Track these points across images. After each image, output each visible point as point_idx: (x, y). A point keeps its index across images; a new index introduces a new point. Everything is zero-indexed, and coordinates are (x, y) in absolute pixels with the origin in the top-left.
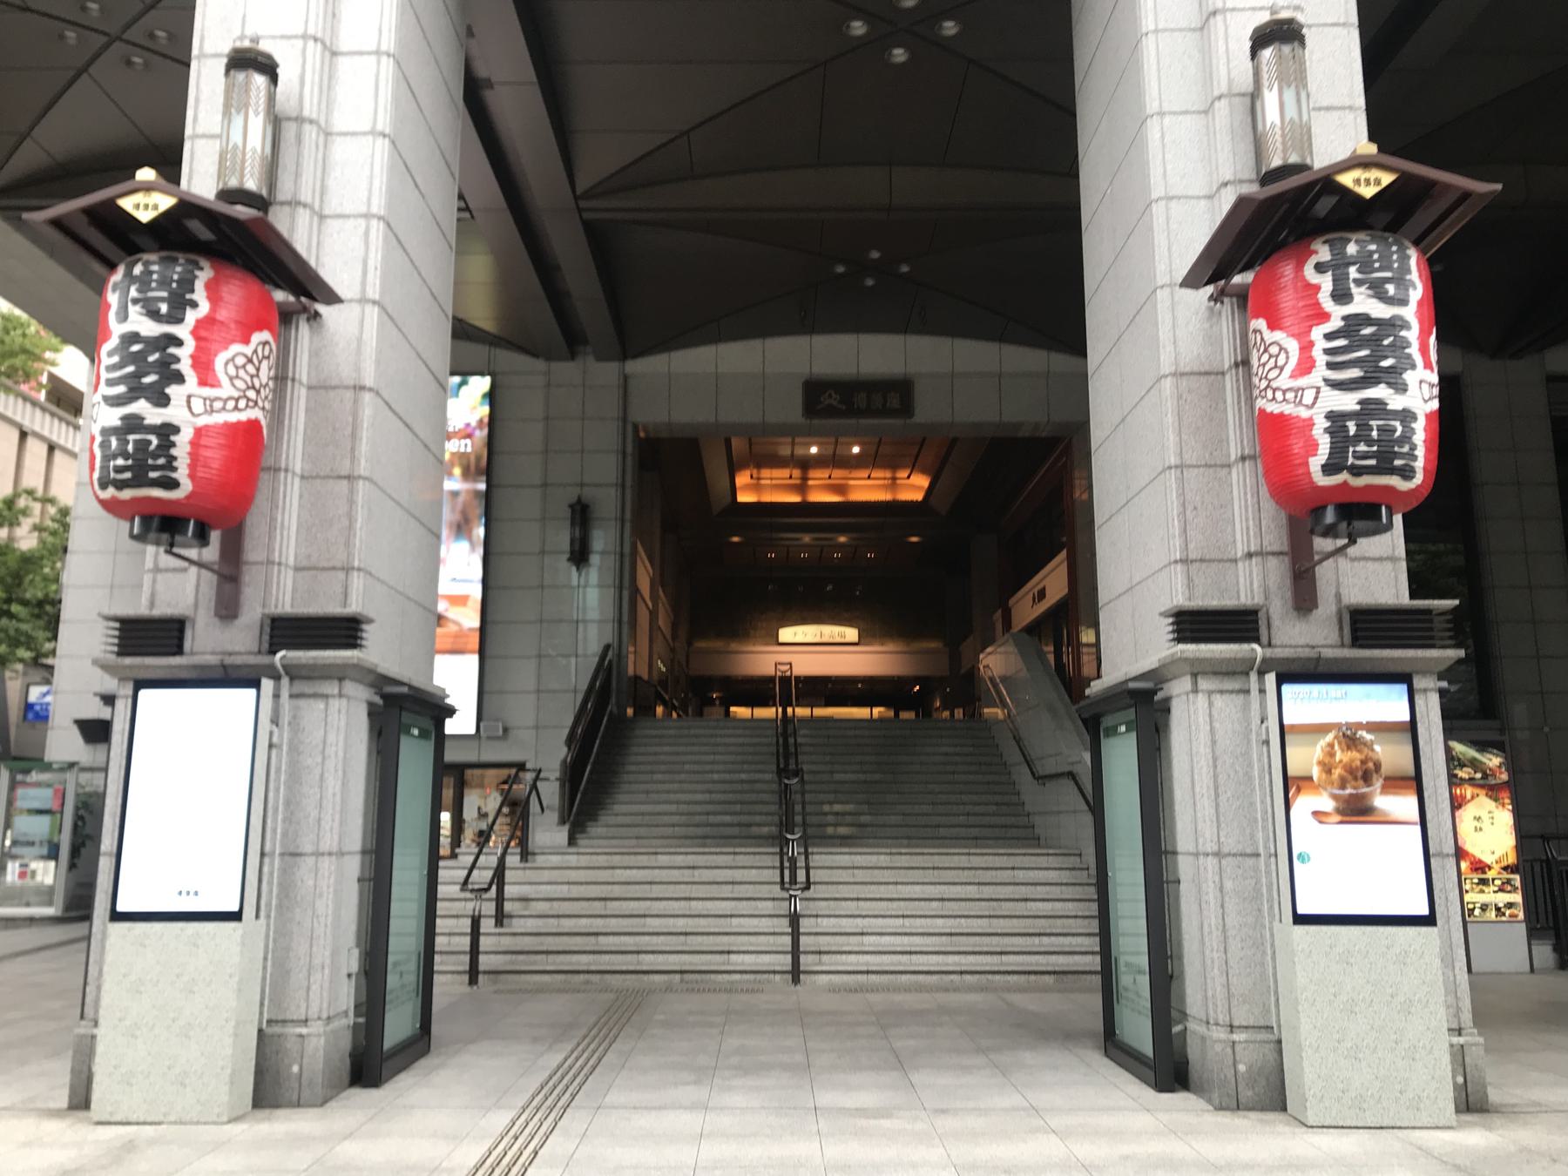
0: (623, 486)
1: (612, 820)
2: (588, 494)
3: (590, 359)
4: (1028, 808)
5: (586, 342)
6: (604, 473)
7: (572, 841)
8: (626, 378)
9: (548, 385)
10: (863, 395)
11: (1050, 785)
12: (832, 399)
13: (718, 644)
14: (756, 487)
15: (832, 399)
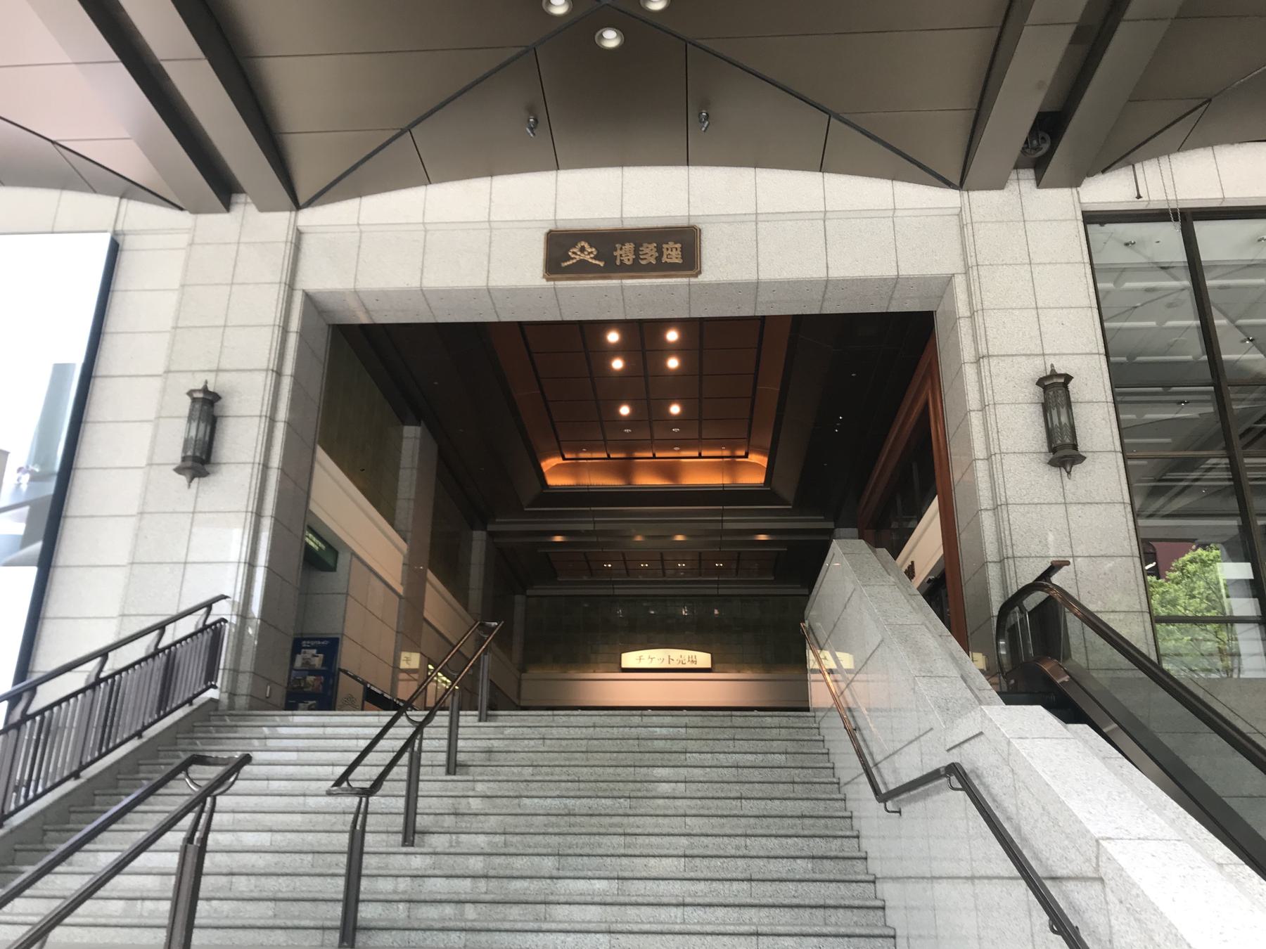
0: (279, 373)
3: (252, 209)
5: (239, 190)
8: (299, 234)
9: (191, 244)
10: (629, 247)
11: (914, 809)
12: (588, 254)
13: (555, 673)
14: (574, 468)
15: (588, 254)
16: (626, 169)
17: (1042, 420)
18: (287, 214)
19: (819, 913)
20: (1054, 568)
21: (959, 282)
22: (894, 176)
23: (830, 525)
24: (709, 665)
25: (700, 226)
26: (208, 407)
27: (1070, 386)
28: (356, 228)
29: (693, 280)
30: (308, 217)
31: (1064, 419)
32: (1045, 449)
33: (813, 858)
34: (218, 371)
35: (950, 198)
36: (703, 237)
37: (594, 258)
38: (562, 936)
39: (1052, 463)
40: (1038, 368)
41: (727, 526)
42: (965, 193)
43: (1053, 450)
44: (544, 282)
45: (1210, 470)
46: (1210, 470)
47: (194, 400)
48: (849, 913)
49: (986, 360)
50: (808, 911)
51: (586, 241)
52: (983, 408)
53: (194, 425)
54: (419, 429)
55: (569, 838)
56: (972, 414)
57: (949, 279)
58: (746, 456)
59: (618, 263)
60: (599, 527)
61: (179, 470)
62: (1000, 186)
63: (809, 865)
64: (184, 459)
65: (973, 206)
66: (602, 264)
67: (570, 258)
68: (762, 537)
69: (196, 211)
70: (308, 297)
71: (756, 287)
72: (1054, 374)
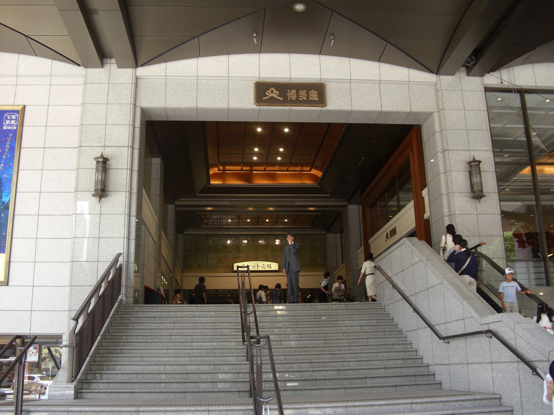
0: (133, 148)
1: (114, 378)
2: (107, 153)
3: (114, 67)
4: (425, 361)
6: (122, 142)
7: (78, 394)
8: (137, 78)
10: (294, 91)
11: (454, 343)
12: (273, 93)
14: (221, 176)
15: (273, 93)
16: (291, 54)
17: (469, 178)
18: (132, 69)
19: (413, 378)
20: (479, 245)
21: (436, 115)
22: (409, 66)
23: (346, 203)
24: (277, 269)
25: (325, 83)
26: (104, 163)
27: (481, 165)
28: (165, 78)
29: (323, 108)
30: (142, 71)
31: (479, 180)
32: (470, 191)
33: (404, 359)
34: (105, 146)
35: (431, 78)
36: (327, 88)
37: (278, 96)
38: (328, 391)
39: (472, 198)
40: (466, 157)
41: (296, 204)
42: (438, 76)
43: (473, 191)
44: (254, 107)
45: (514, 182)
46: (514, 182)
47: (98, 162)
48: (423, 377)
49: (447, 152)
50: (409, 377)
51: (274, 87)
52: (445, 172)
53: (100, 174)
54: (159, 159)
55: (309, 356)
56: (441, 174)
57: (432, 113)
58: (310, 170)
59: (289, 99)
60: (232, 203)
61: (93, 195)
62: (452, 74)
63: (402, 362)
64: (96, 190)
65: (442, 82)
66: (282, 99)
67: (266, 96)
68: (312, 209)
69: (86, 66)
70: (143, 110)
71: (350, 112)
72: (474, 161)
